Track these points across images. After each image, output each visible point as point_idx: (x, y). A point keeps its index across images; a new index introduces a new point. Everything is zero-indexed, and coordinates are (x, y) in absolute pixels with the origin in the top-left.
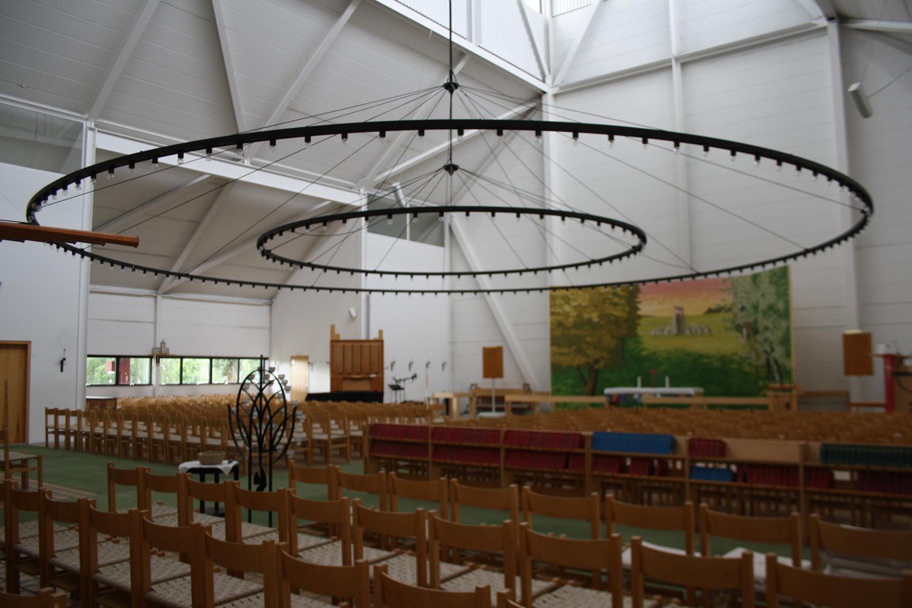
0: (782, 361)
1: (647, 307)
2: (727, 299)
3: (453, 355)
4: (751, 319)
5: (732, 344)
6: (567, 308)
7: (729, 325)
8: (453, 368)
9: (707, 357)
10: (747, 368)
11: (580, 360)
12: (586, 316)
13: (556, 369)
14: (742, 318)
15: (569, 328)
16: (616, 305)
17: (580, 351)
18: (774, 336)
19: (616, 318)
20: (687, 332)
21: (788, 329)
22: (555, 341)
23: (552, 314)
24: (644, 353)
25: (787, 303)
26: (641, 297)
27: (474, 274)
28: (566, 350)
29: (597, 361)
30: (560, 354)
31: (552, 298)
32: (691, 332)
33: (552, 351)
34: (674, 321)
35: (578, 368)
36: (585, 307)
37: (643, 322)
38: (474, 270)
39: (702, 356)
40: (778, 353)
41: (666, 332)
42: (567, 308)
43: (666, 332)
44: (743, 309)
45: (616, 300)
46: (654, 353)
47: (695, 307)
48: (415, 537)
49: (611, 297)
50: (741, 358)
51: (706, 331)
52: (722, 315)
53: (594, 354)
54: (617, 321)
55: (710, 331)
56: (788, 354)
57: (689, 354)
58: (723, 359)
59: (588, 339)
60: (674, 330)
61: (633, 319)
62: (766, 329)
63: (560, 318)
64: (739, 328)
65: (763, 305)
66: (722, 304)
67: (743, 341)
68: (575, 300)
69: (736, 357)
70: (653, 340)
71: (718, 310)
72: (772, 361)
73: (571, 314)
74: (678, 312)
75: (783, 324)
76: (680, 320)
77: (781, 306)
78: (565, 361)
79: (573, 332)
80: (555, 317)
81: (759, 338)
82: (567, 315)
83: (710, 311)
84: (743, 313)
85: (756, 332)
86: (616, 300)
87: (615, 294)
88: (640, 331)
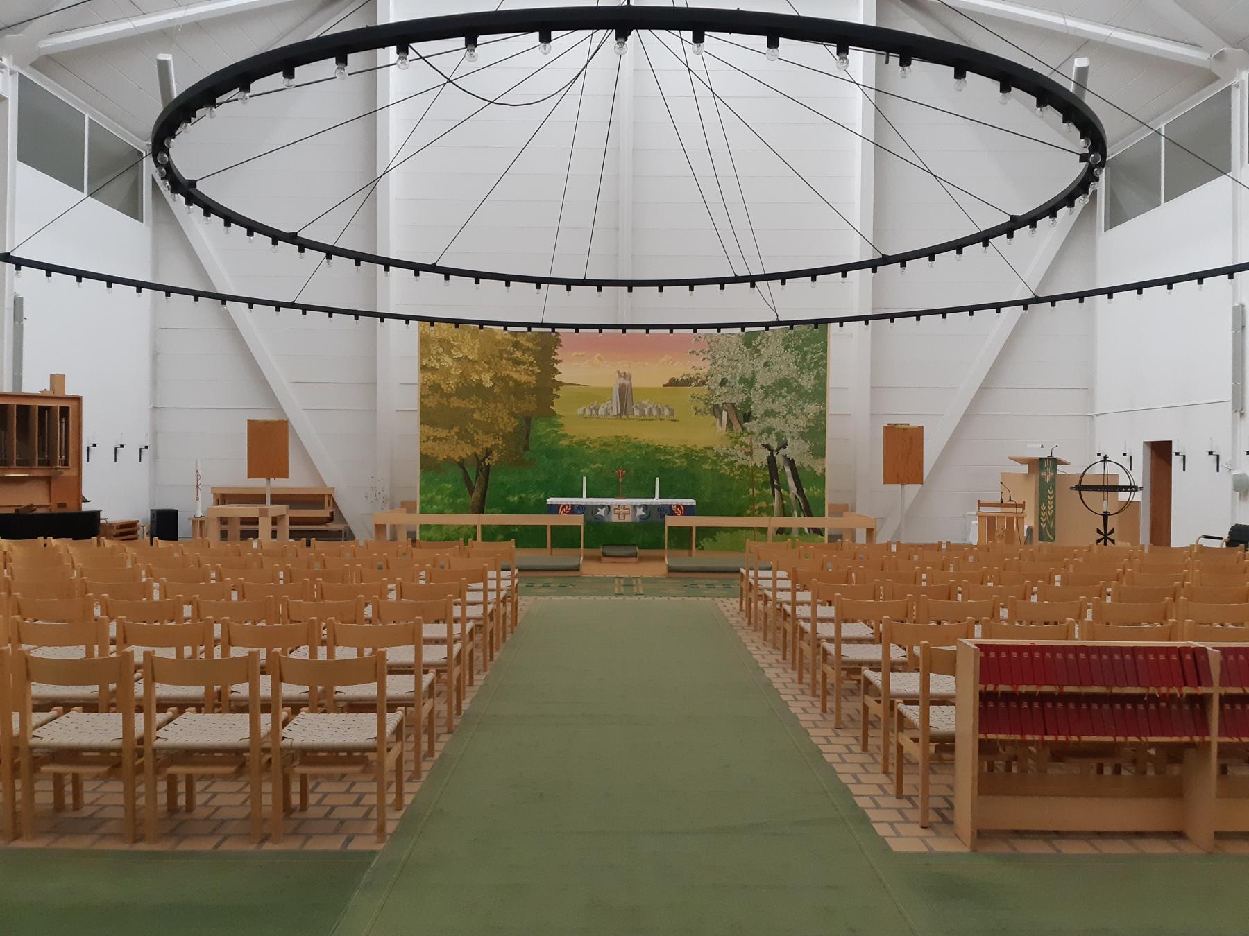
0: (803, 461)
1: (576, 369)
2: (702, 367)
3: (155, 433)
4: (738, 399)
5: (709, 435)
6: (447, 361)
7: (701, 405)
8: (155, 458)
9: (665, 451)
10: (725, 470)
11: (464, 451)
12: (475, 377)
13: (428, 464)
14: (722, 397)
15: (449, 396)
16: (517, 362)
17: (465, 436)
18: (790, 426)
19: (518, 384)
20: (637, 413)
21: (823, 414)
22: (428, 417)
23: (424, 368)
24: (564, 443)
25: (822, 381)
26: (560, 354)
27: (224, 299)
28: (443, 433)
29: (488, 453)
30: (435, 439)
31: (424, 341)
32: (642, 412)
33: (422, 433)
34: (616, 395)
35: (461, 464)
36: (473, 362)
37: (562, 392)
38: (221, 290)
39: (658, 449)
40: (797, 450)
41: (601, 411)
42: (447, 361)
43: (601, 411)
44: (723, 383)
45: (518, 354)
46: (581, 443)
47: (650, 374)
48: (16, 716)
49: (511, 349)
50: (718, 455)
51: (666, 412)
52: (692, 390)
53: (486, 441)
54: (519, 390)
55: (672, 412)
56: (819, 452)
57: (638, 447)
58: (689, 454)
59: (476, 416)
60: (616, 410)
61: (547, 387)
62: (769, 413)
63: (435, 377)
64: (716, 411)
65: (765, 378)
66: (693, 374)
67: (722, 429)
68: (459, 348)
69: (709, 453)
70: (578, 423)
71: (687, 382)
72: (779, 460)
73: (452, 371)
74: (622, 381)
75: (812, 408)
76: (625, 394)
77: (807, 382)
78: (442, 452)
79: (455, 402)
80: (428, 375)
81: (751, 426)
82: (446, 373)
83: (673, 383)
84: (725, 389)
85: (748, 417)
86: (518, 354)
87: (516, 345)
88: (557, 407)
